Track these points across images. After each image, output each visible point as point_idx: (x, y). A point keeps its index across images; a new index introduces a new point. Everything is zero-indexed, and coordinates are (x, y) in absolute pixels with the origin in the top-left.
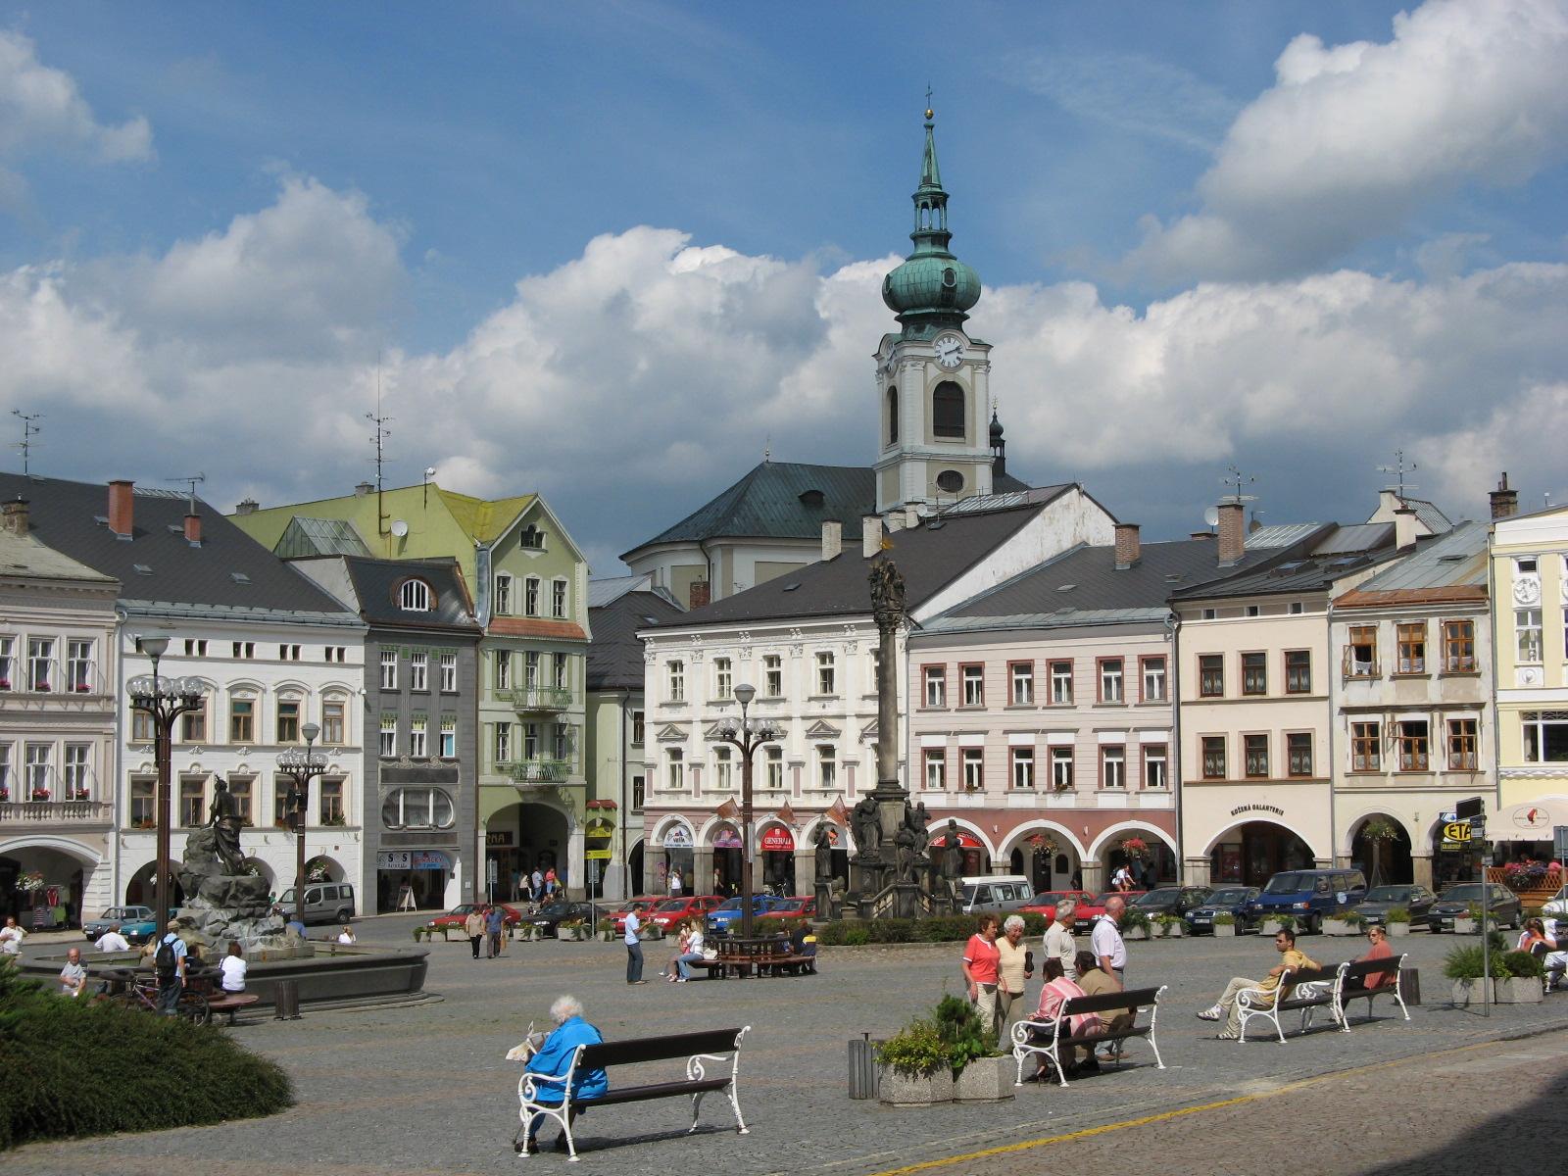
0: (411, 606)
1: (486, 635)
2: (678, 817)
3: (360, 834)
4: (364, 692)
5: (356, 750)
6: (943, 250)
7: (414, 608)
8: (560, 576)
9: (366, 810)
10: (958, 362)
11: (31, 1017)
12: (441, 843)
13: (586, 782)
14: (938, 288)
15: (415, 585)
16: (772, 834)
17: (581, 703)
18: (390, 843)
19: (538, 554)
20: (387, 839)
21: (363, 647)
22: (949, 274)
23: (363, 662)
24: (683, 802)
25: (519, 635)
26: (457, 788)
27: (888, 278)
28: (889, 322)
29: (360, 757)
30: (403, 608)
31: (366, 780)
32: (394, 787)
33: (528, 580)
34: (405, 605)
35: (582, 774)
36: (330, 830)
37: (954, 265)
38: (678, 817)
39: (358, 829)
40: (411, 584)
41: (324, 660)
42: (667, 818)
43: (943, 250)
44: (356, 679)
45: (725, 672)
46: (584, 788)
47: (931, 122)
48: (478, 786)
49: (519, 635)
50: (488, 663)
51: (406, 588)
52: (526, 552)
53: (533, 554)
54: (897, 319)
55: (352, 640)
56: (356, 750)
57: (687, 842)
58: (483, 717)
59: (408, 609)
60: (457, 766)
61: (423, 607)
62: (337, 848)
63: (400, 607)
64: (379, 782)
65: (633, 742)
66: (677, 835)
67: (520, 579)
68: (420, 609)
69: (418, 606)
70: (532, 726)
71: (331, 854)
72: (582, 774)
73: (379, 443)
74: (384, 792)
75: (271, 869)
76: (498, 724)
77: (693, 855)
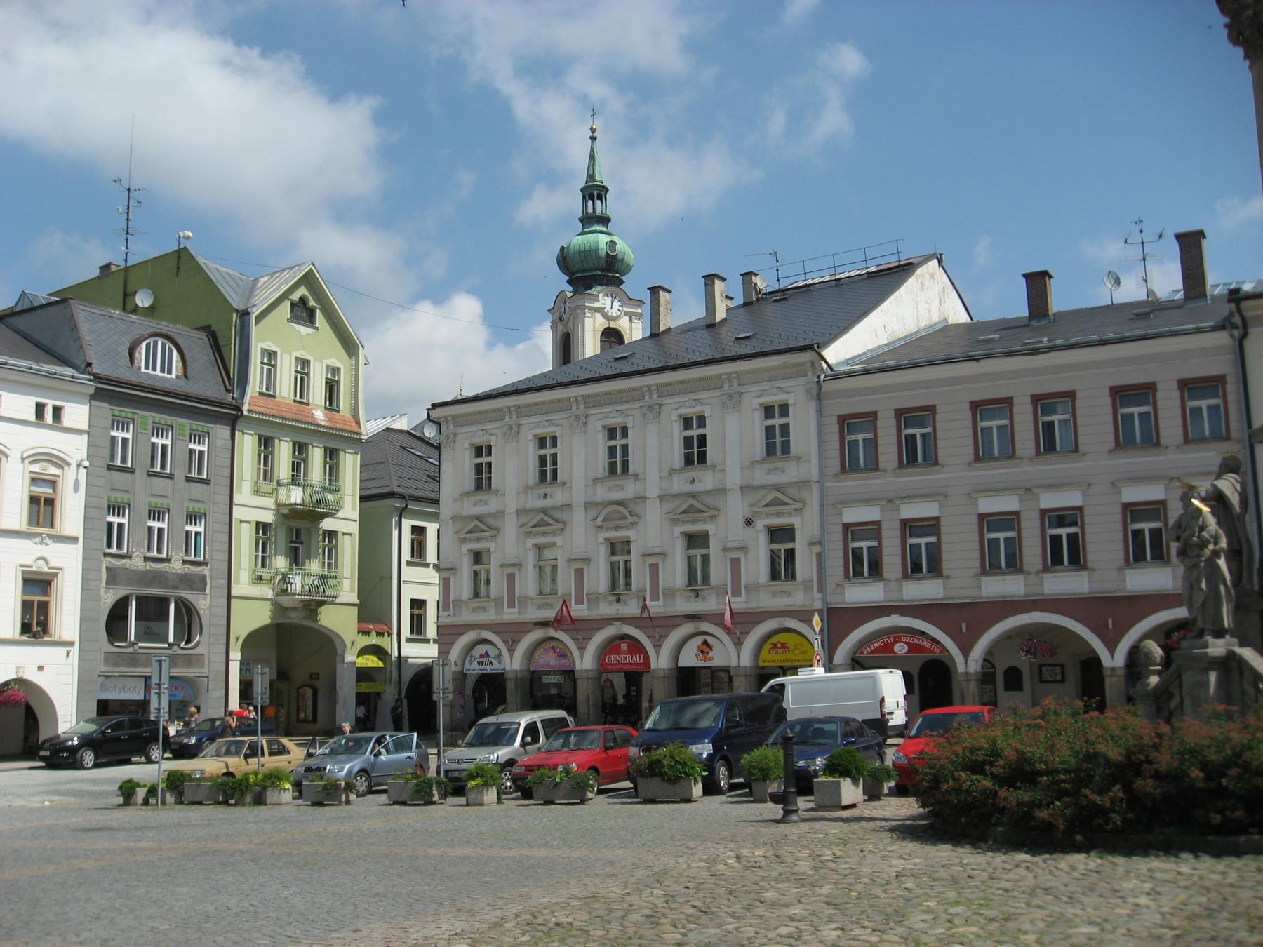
0: (154, 369)
1: (245, 413)
2: (487, 635)
3: (75, 650)
4: (87, 464)
5: (73, 540)
6: (605, 229)
7: (158, 372)
8: (333, 360)
9: (83, 620)
10: (619, 313)
11: (500, 655)
12: (183, 667)
13: (357, 602)
14: (603, 253)
15: (160, 343)
16: (617, 651)
17: (353, 508)
18: (116, 664)
19: (310, 330)
20: (110, 659)
21: (87, 407)
22: (613, 243)
23: (85, 427)
24: (490, 616)
25: (286, 419)
26: (205, 600)
27: (563, 248)
28: (561, 282)
29: (77, 550)
30: (143, 370)
31: (85, 580)
32: (122, 593)
33: (297, 358)
34: (147, 367)
35: (354, 591)
36: (33, 644)
37: (616, 239)
38: (487, 635)
39: (71, 644)
40: (156, 344)
41: (32, 417)
42: (470, 636)
43: (605, 229)
44: (75, 448)
45: (548, 451)
46: (356, 608)
47: (595, 134)
48: (229, 597)
49: (286, 419)
50: (247, 444)
51: (148, 346)
52: (297, 327)
53: (305, 330)
54: (568, 282)
55: (74, 397)
56: (73, 540)
57: (496, 664)
58: (238, 513)
59: (150, 372)
60: (205, 571)
61: (170, 372)
62: (41, 668)
63: (140, 368)
64: (104, 584)
65: (409, 559)
66: (481, 656)
67: (288, 356)
68: (166, 375)
69: (162, 371)
70: (298, 531)
71: (31, 675)
72: (354, 591)
73: (128, 213)
74: (109, 598)
75: (934, 844)
76: (258, 524)
77: (505, 680)
